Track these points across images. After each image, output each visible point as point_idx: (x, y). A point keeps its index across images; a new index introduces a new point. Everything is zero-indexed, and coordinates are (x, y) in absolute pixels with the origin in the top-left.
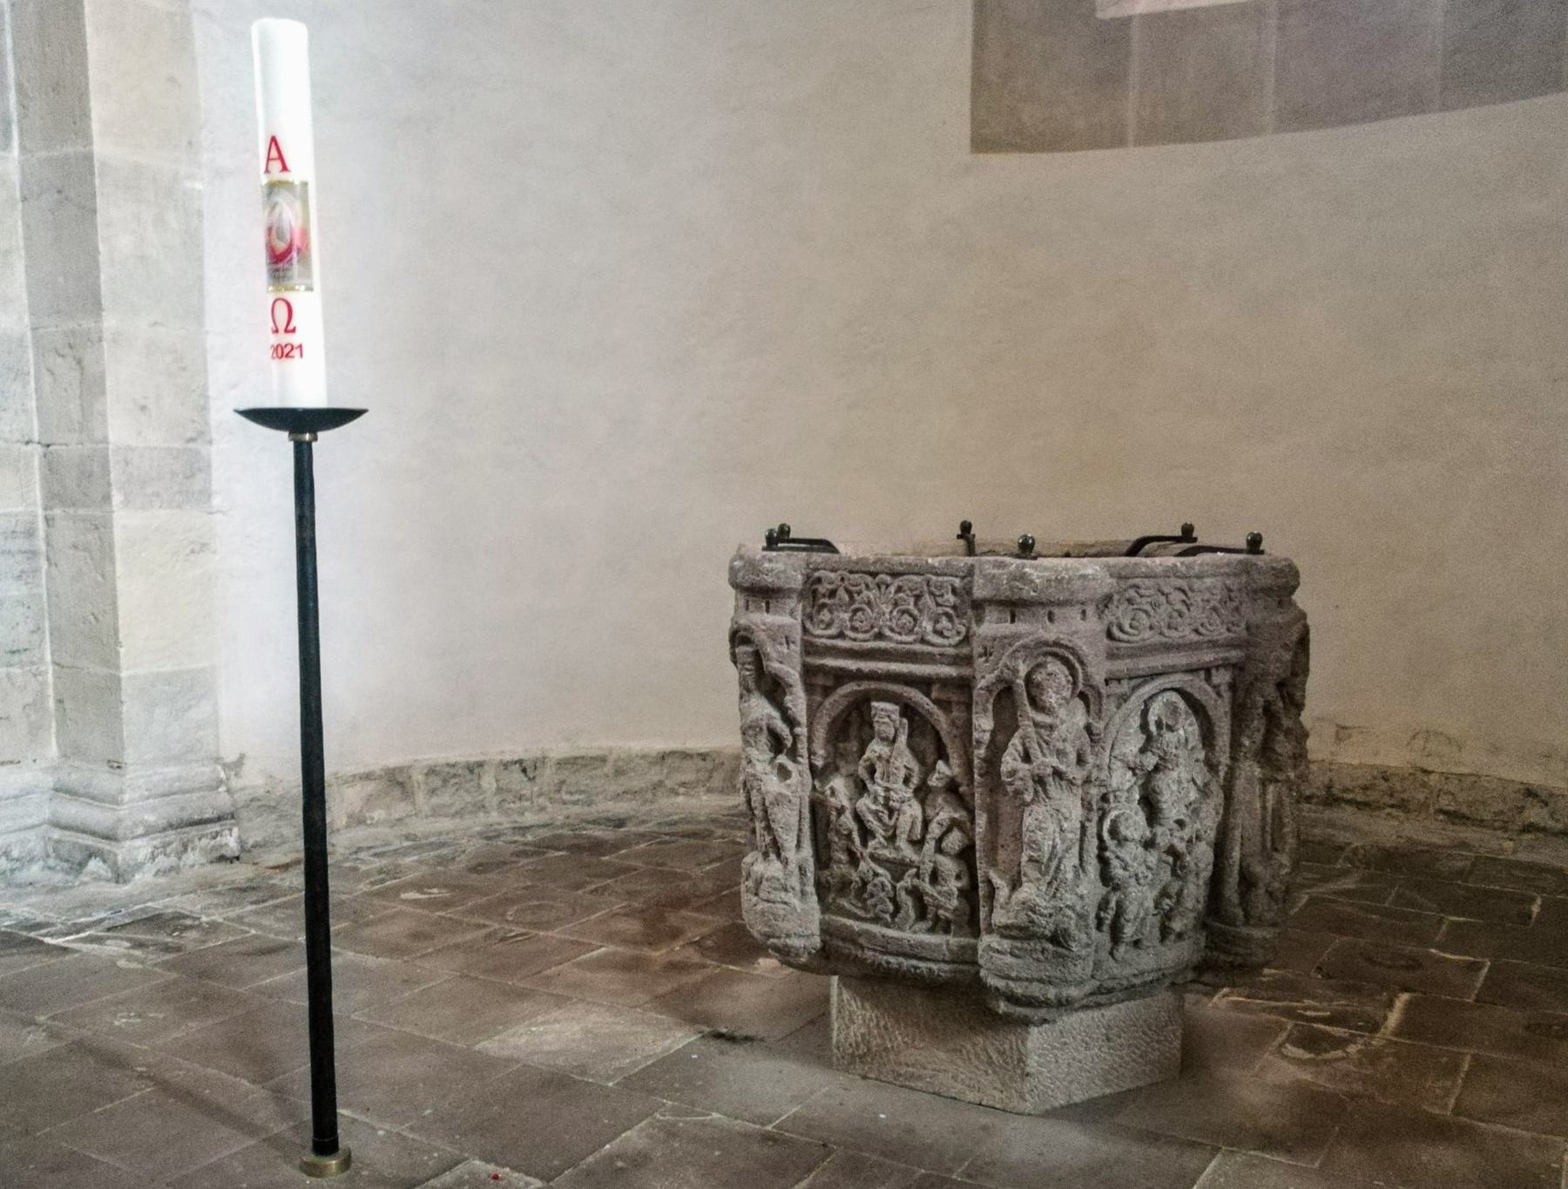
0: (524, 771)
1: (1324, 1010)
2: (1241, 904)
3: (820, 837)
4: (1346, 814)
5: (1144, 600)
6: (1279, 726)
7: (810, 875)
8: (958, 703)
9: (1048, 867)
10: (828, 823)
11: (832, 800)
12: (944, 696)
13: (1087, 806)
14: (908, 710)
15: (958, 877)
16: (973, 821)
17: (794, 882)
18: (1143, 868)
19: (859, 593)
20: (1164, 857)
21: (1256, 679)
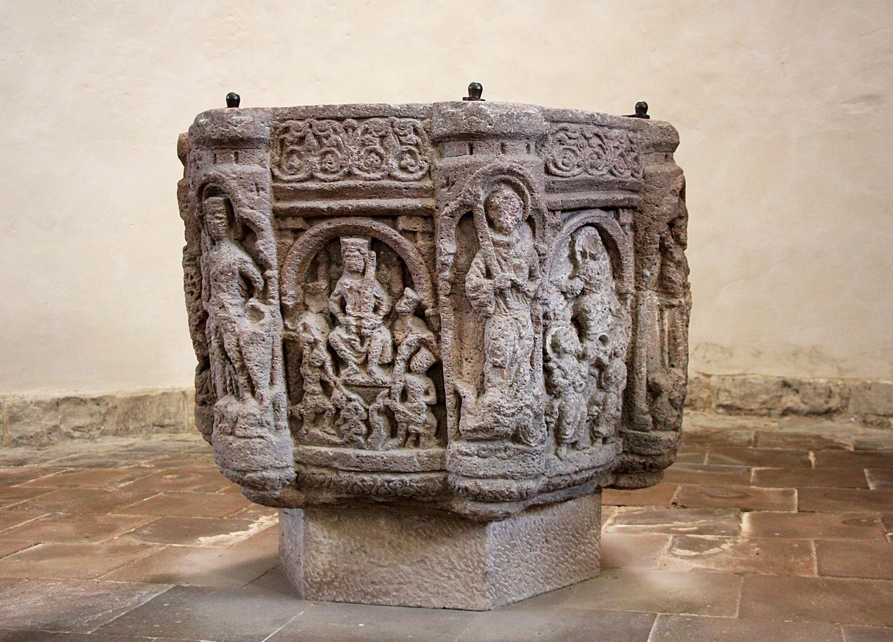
3: (292, 374)
5: (572, 142)
8: (423, 233)
10: (301, 356)
14: (376, 243)
16: (438, 339)
17: (269, 417)
18: (578, 377)
19: (327, 137)
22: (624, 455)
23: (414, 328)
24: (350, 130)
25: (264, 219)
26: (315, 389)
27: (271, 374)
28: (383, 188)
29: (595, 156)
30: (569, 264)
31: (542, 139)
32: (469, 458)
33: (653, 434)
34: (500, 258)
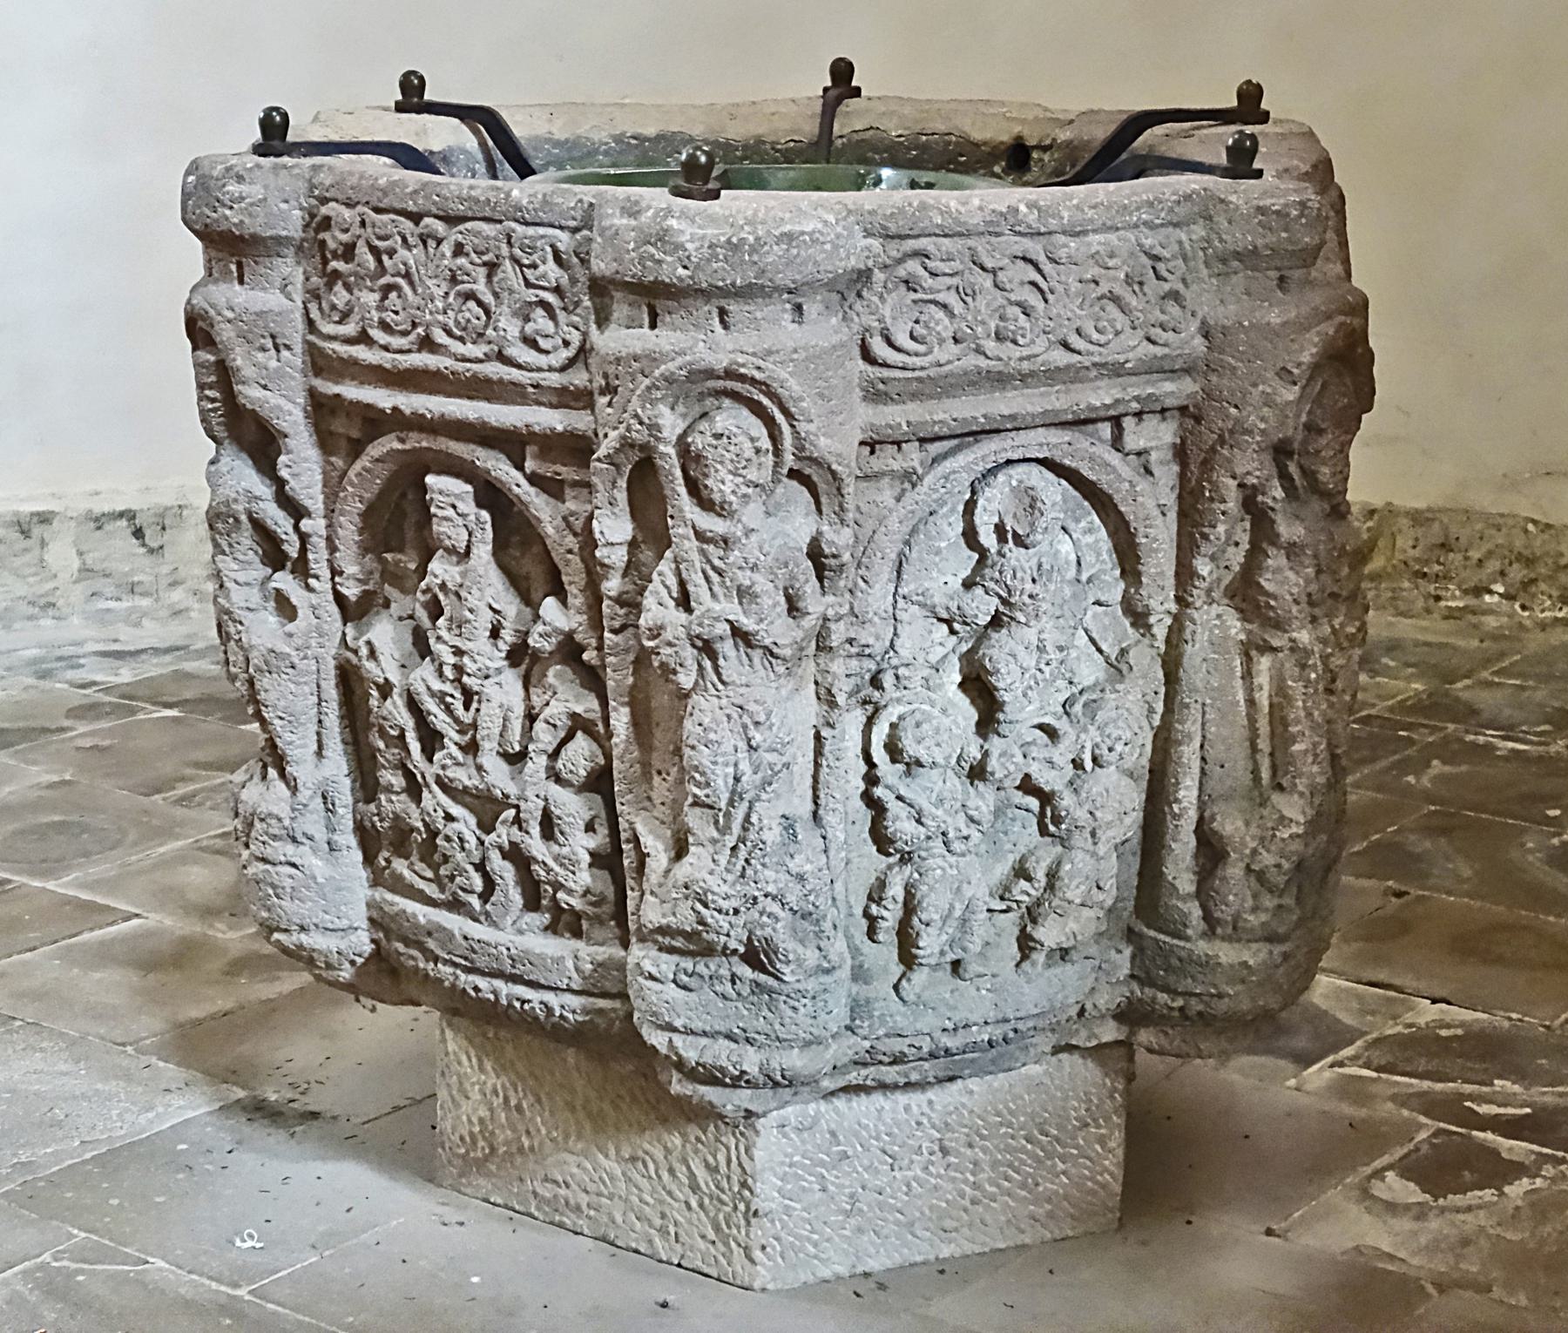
0: (138, 533)
6: (1274, 539)
9: (728, 815)
11: (369, 665)
12: (547, 470)
14: (490, 495)
15: (590, 828)
17: (313, 823)
19: (391, 253)
21: (1222, 441)
23: (560, 689)
24: (432, 243)
25: (287, 410)
26: (394, 781)
27: (318, 734)
28: (488, 381)
34: (708, 568)
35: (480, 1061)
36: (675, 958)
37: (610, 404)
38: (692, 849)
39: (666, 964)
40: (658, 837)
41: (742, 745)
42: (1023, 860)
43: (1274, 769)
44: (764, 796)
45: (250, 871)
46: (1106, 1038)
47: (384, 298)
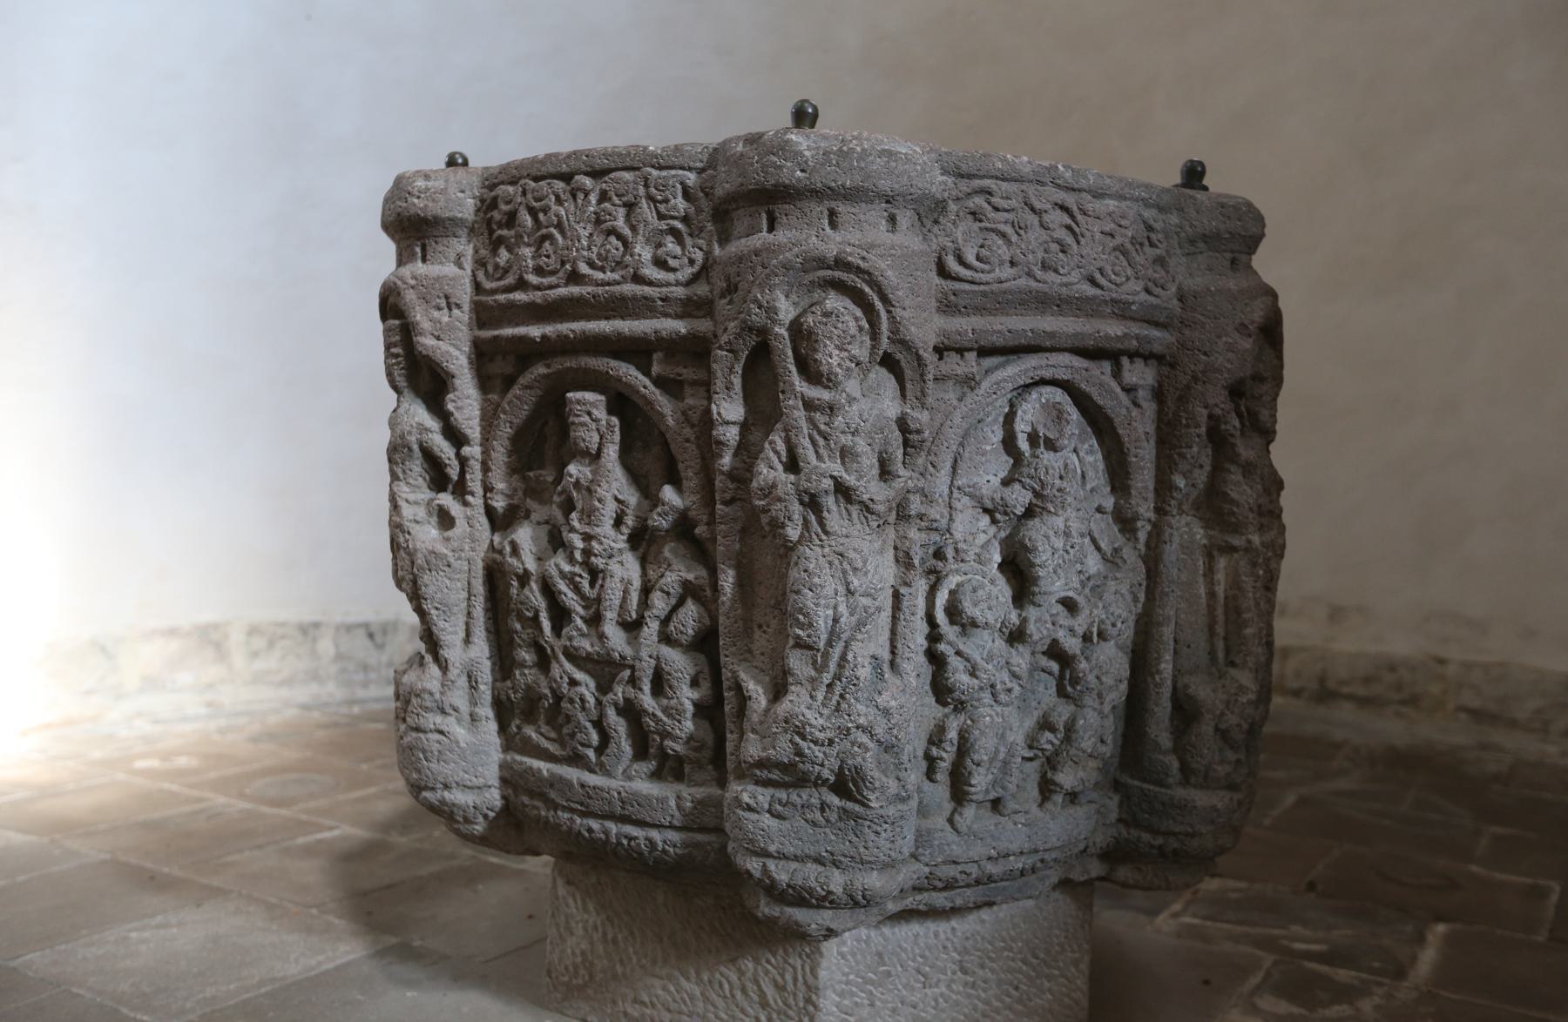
0: (371, 636)
1: (1317, 942)
2: (1175, 750)
4: (1345, 712)
6: (1234, 458)
7: (486, 691)
9: (826, 655)
12: (670, 371)
13: (904, 560)
14: (622, 402)
15: (694, 683)
18: (1006, 676)
20: (1045, 662)
21: (1195, 379)
22: (1121, 826)
23: (674, 561)
25: (456, 357)
27: (467, 624)
28: (623, 299)
29: (1055, 247)
30: (1005, 457)
31: (931, 211)
32: (754, 816)
33: (1180, 793)
35: (583, 900)
36: (770, 791)
37: (730, 302)
38: (793, 688)
39: (763, 796)
40: (758, 682)
41: (842, 590)
42: (1045, 716)
43: (1228, 650)
44: (859, 637)
45: (407, 740)
46: (1094, 874)
47: (539, 247)
